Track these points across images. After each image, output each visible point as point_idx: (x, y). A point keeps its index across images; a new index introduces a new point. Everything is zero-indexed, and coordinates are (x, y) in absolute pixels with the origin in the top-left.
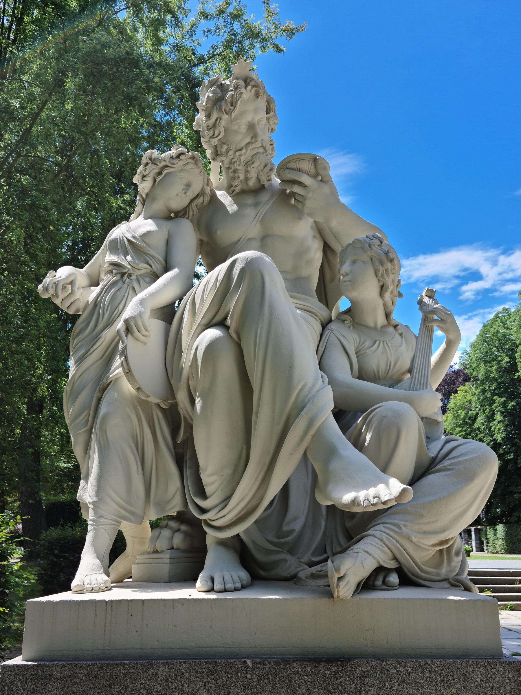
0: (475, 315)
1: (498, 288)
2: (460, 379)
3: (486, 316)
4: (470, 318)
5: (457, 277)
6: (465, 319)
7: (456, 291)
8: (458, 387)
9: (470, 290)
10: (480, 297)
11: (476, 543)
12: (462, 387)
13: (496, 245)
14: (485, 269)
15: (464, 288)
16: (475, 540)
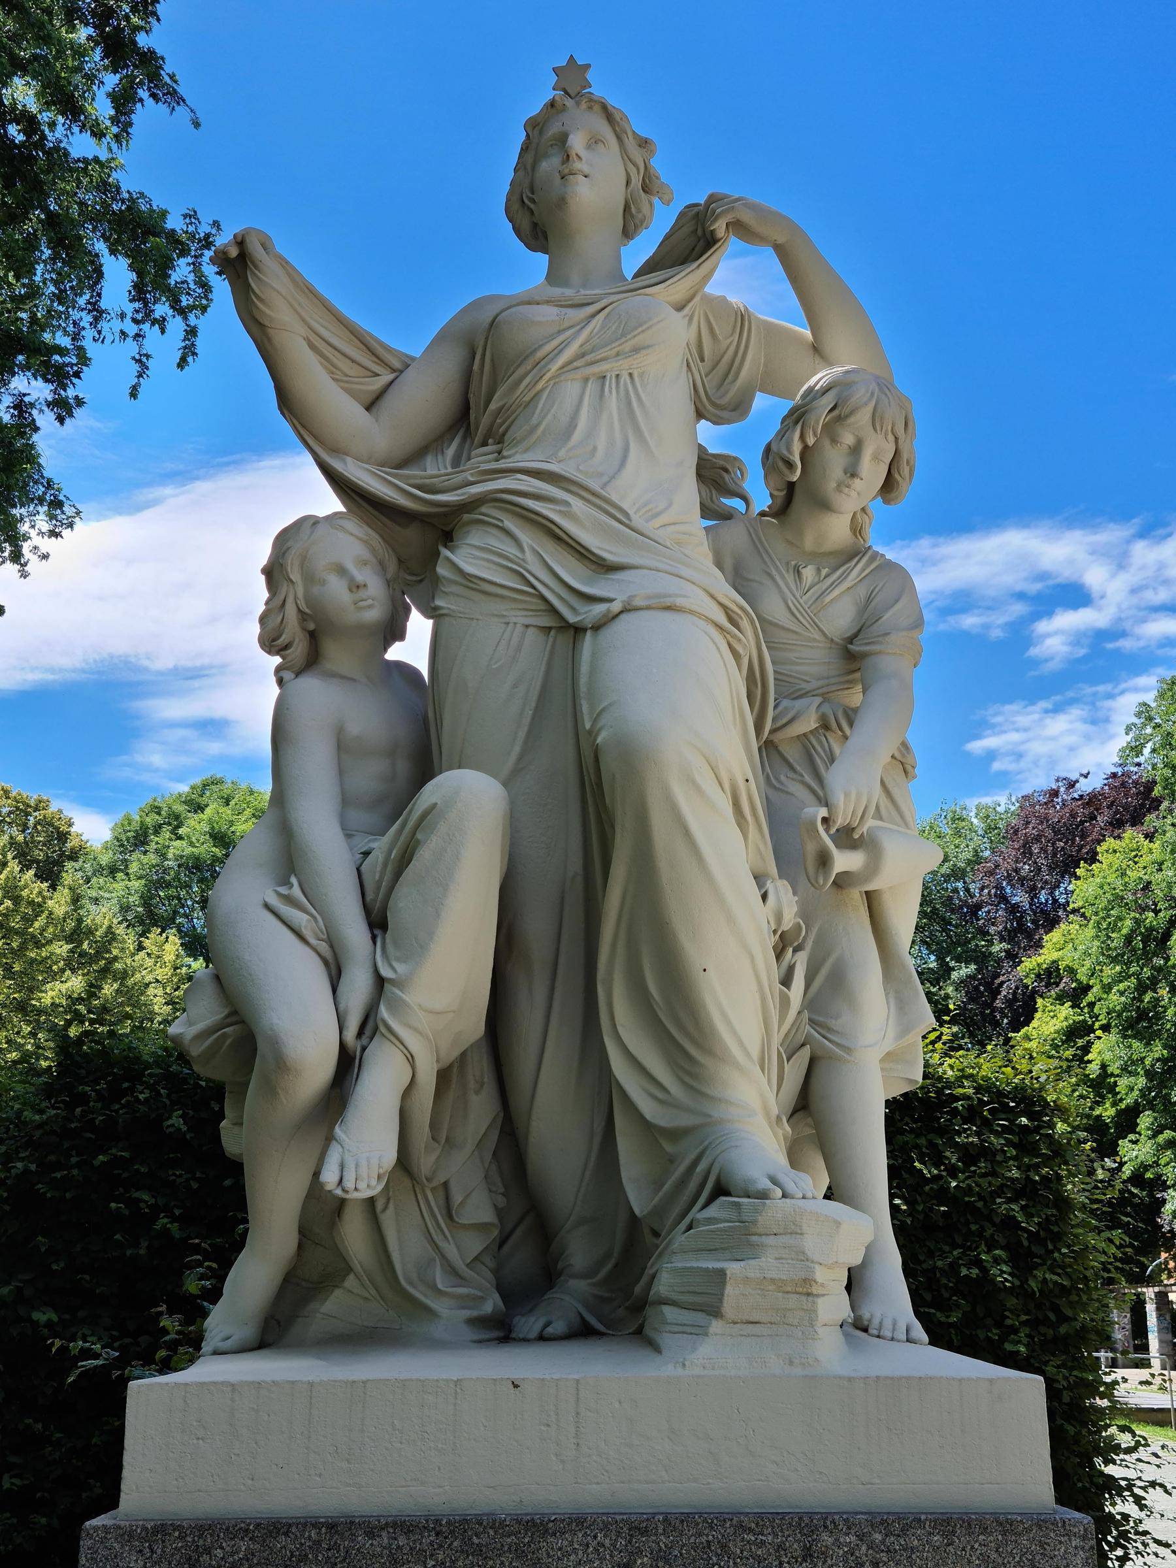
0: (1072, 702)
1: (1127, 625)
2: (1101, 820)
3: (1099, 704)
4: (1057, 709)
5: (1021, 596)
6: (1046, 711)
7: (1020, 635)
8: (1099, 842)
9: (1058, 633)
10: (1082, 652)
11: (1161, 1341)
12: (1110, 843)
13: (1122, 515)
14: (1095, 577)
15: (1043, 626)
16: (1159, 1331)
